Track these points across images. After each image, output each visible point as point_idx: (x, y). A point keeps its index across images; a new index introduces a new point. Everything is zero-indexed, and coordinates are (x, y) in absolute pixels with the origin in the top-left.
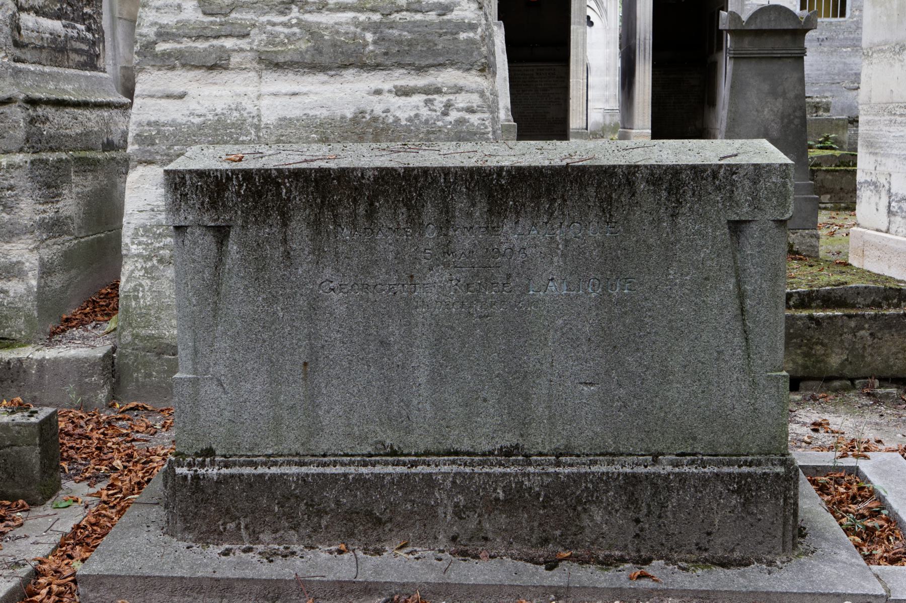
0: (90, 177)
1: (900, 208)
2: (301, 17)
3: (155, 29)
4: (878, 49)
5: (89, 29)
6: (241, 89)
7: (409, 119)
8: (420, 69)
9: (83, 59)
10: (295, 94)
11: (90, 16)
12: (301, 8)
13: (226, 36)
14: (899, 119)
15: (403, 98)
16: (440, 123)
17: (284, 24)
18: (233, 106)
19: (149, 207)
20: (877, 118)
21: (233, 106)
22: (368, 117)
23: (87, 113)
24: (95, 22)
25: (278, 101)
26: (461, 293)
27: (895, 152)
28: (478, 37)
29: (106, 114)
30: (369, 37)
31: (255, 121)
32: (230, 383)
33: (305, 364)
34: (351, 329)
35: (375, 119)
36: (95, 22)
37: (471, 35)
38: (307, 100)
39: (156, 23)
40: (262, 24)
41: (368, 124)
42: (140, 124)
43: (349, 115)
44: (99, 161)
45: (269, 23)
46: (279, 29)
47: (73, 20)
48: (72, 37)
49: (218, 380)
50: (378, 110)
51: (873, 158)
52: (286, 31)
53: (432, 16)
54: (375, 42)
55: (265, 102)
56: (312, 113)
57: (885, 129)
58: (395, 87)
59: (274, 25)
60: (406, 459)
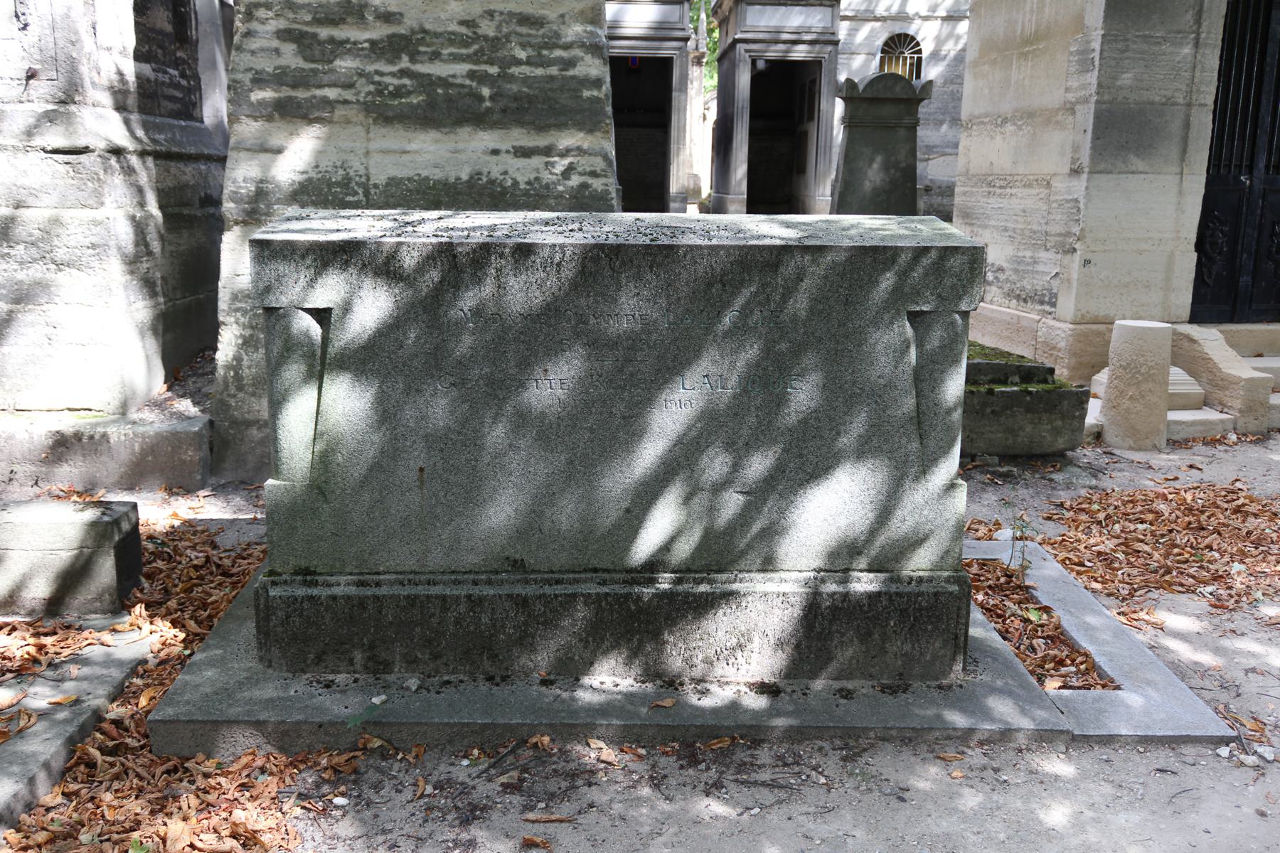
0: (185, 235)
1: (996, 278)
3: (250, 75)
4: (974, 121)
5: (183, 75)
6: (347, 145)
7: (529, 183)
8: (542, 129)
10: (405, 152)
11: (184, 62)
14: (998, 191)
15: (522, 160)
16: (560, 188)
17: (393, 74)
18: (339, 164)
21: (339, 164)
22: (485, 179)
23: (181, 165)
24: (190, 68)
25: (388, 159)
26: (603, 390)
27: (992, 223)
28: (602, 96)
29: (203, 167)
30: (486, 92)
31: (363, 179)
33: (421, 470)
35: (492, 182)
36: (190, 68)
37: (595, 93)
38: (419, 158)
39: (251, 69)
41: (484, 187)
43: (465, 177)
44: (195, 217)
45: (377, 72)
47: (164, 63)
48: (163, 83)
50: (496, 173)
51: (969, 229)
53: (554, 71)
54: (492, 98)
55: (374, 160)
58: (514, 147)
59: (382, 74)
60: (539, 576)
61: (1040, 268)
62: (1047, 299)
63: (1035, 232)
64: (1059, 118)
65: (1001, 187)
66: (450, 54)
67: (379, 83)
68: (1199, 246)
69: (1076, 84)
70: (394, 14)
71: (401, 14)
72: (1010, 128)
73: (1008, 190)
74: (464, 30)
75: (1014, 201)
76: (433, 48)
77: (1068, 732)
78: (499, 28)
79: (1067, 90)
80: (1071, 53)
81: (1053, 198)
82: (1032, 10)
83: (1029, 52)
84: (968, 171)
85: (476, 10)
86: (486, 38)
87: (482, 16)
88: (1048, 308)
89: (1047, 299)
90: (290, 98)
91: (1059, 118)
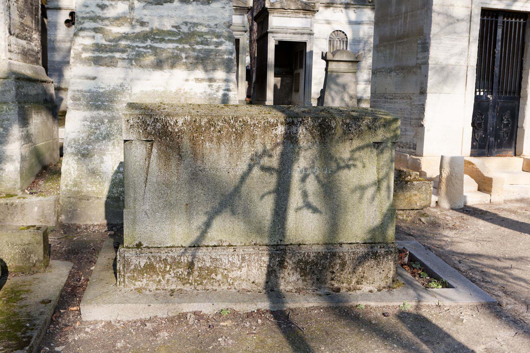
2: (152, 45)
3: (82, 46)
9: (33, 59)
12: (152, 41)
13: (116, 52)
14: (389, 100)
16: (215, 96)
18: (119, 85)
19: (77, 130)
20: (379, 100)
22: (182, 92)
28: (233, 58)
32: (151, 214)
33: (187, 204)
34: (209, 189)
39: (82, 44)
40: (133, 47)
42: (74, 91)
43: (174, 91)
45: (137, 46)
46: (141, 49)
49: (145, 212)
52: (145, 50)
53: (212, 47)
54: (186, 58)
56: (156, 89)
57: (382, 104)
59: (139, 47)
61: (408, 133)
62: (412, 146)
63: (406, 118)
64: (414, 70)
65: (390, 99)
66: (168, 40)
67: (138, 51)
68: (473, 124)
69: (421, 57)
70: (145, 23)
71: (148, 23)
72: (393, 74)
73: (394, 100)
74: (174, 30)
75: (396, 105)
76: (161, 37)
77: (34, 226)
78: (189, 29)
79: (417, 59)
80: (418, 44)
81: (413, 104)
82: (401, 25)
83: (401, 42)
84: (375, 91)
85: (180, 21)
86: (184, 33)
87: (182, 24)
88: (412, 150)
89: (412, 146)
90: (99, 56)
91: (414, 70)
